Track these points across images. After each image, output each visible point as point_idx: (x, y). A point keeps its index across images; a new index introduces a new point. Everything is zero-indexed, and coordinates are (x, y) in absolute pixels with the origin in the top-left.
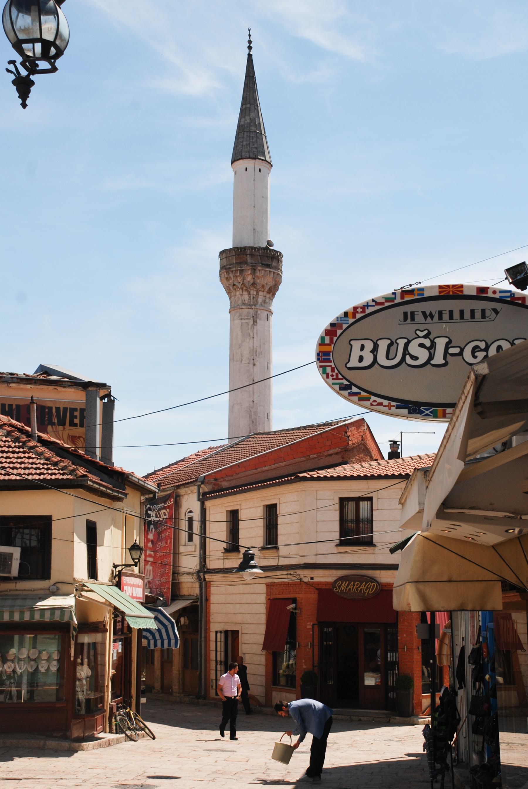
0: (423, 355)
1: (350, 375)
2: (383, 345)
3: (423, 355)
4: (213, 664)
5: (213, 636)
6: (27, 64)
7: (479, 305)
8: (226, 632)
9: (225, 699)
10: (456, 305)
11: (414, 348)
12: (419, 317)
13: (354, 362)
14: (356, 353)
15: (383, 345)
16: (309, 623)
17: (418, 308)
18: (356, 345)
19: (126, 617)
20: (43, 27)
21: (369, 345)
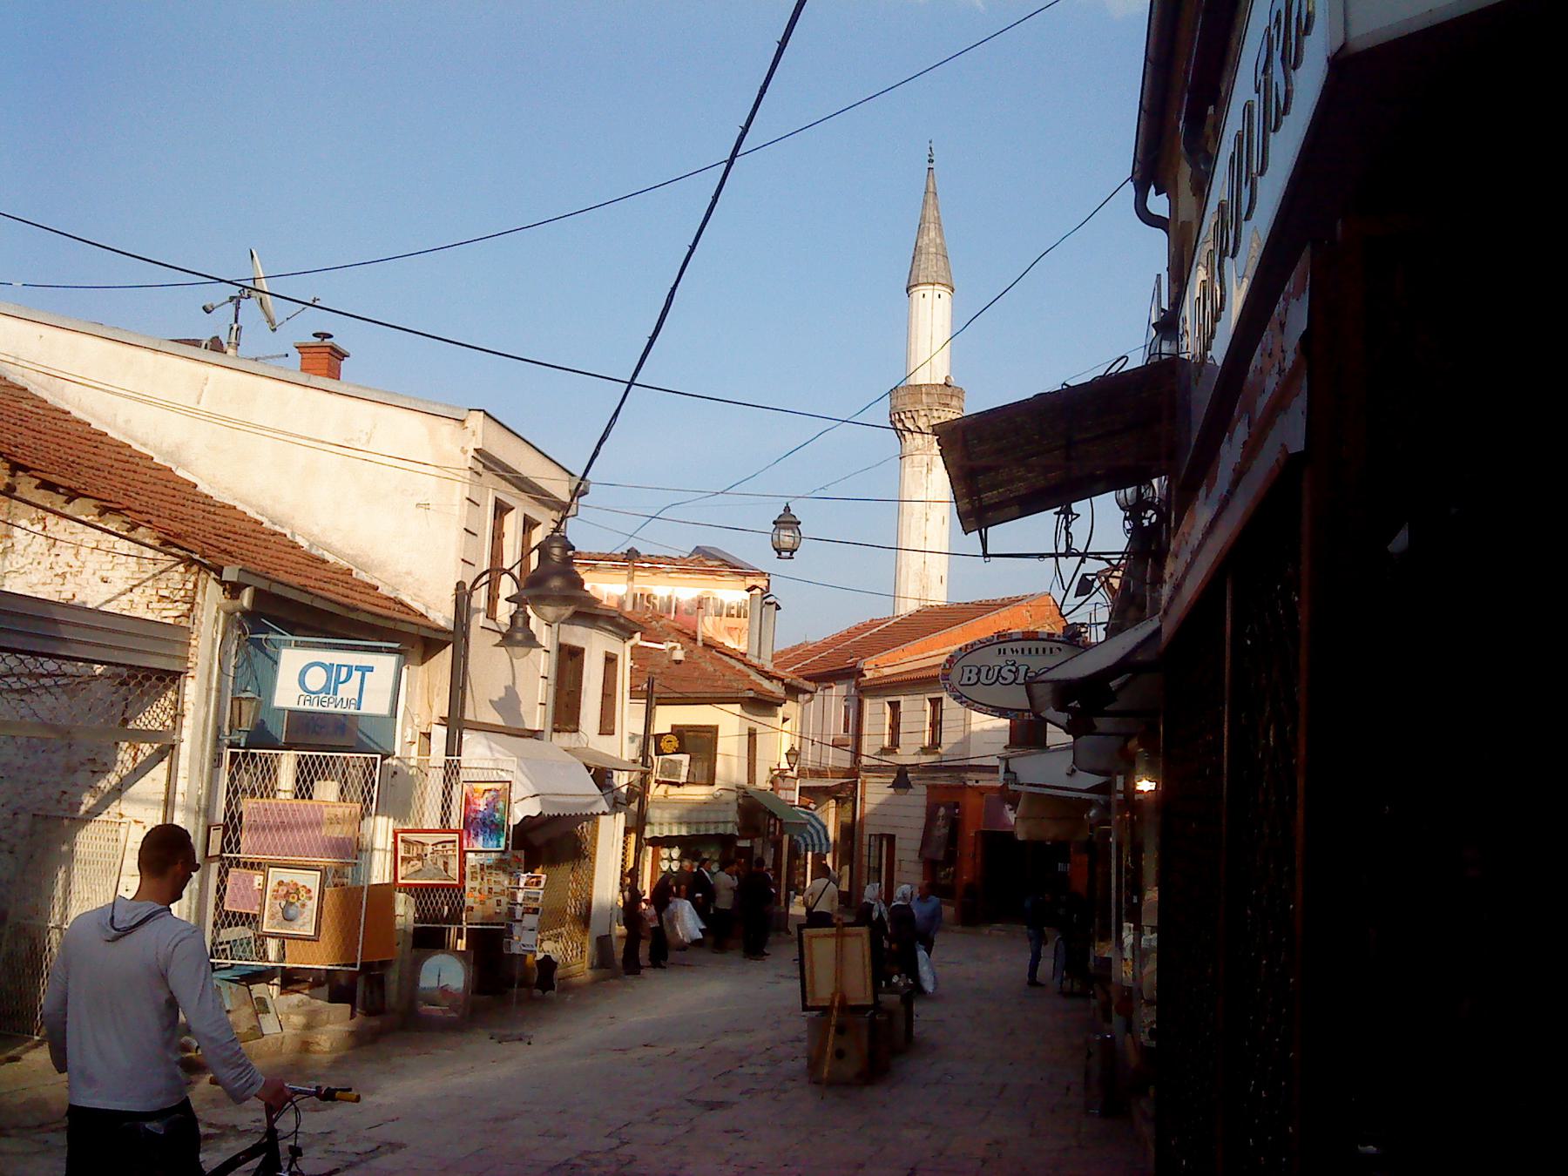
0: (1011, 677)
1: (961, 689)
2: (984, 670)
3: (1011, 677)
4: (866, 871)
5: (866, 839)
6: (1371, 1148)
7: (1048, 645)
8: (882, 836)
9: (1057, 566)
10: (1033, 645)
11: (1004, 673)
12: (1008, 652)
13: (965, 681)
14: (966, 675)
15: (984, 670)
16: (1154, 519)
17: (1008, 646)
18: (967, 670)
19: (76, 601)
20: (163, 788)
21: (975, 670)
